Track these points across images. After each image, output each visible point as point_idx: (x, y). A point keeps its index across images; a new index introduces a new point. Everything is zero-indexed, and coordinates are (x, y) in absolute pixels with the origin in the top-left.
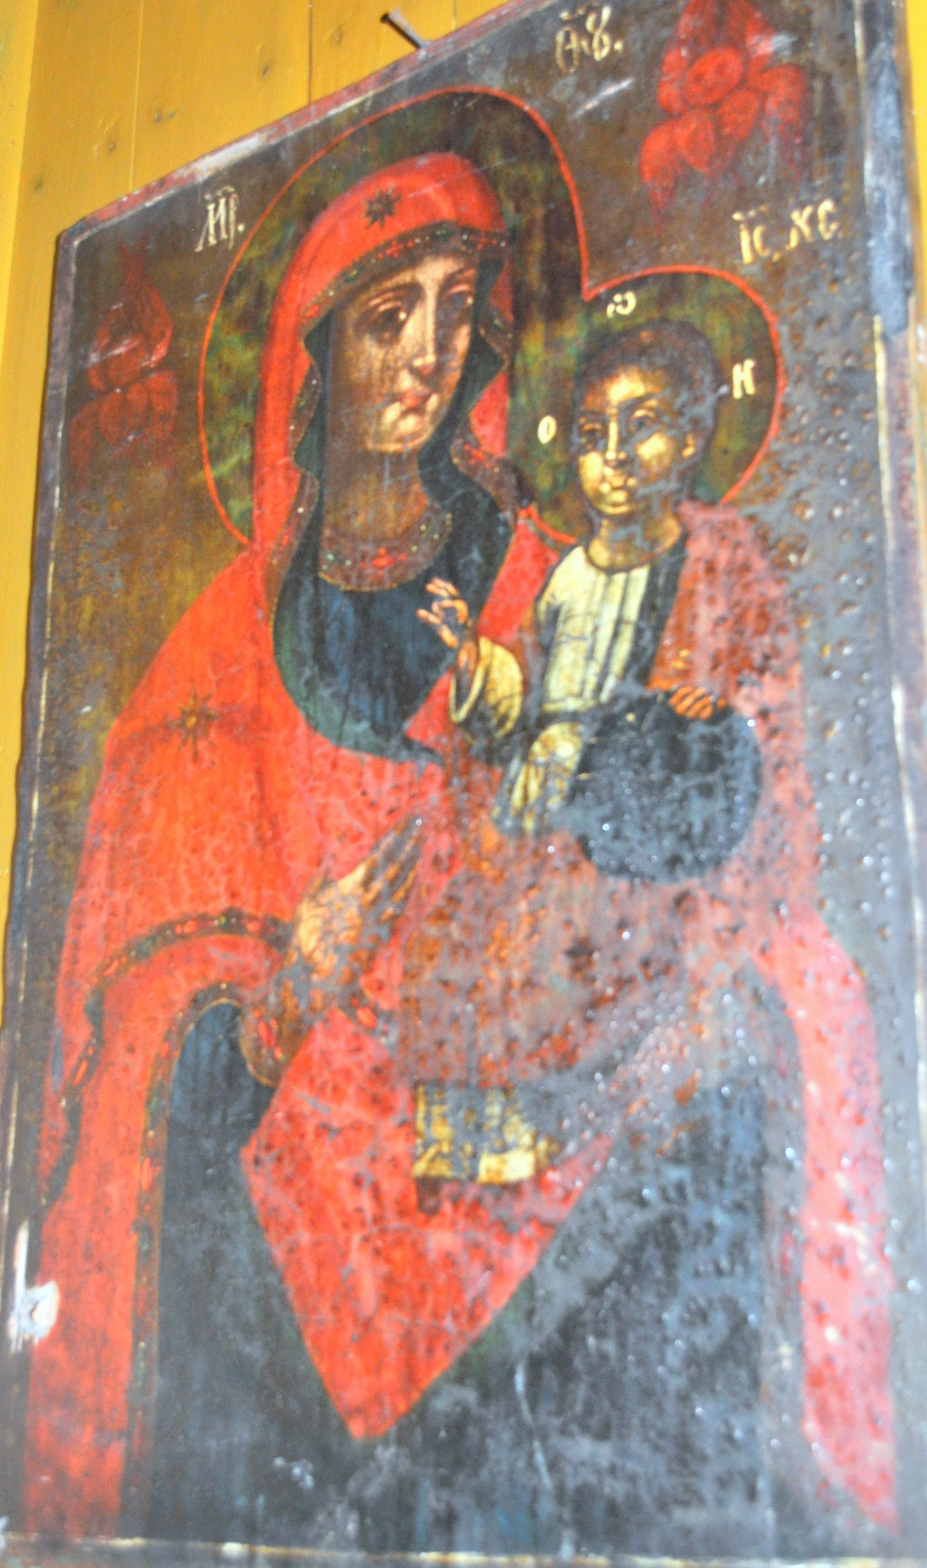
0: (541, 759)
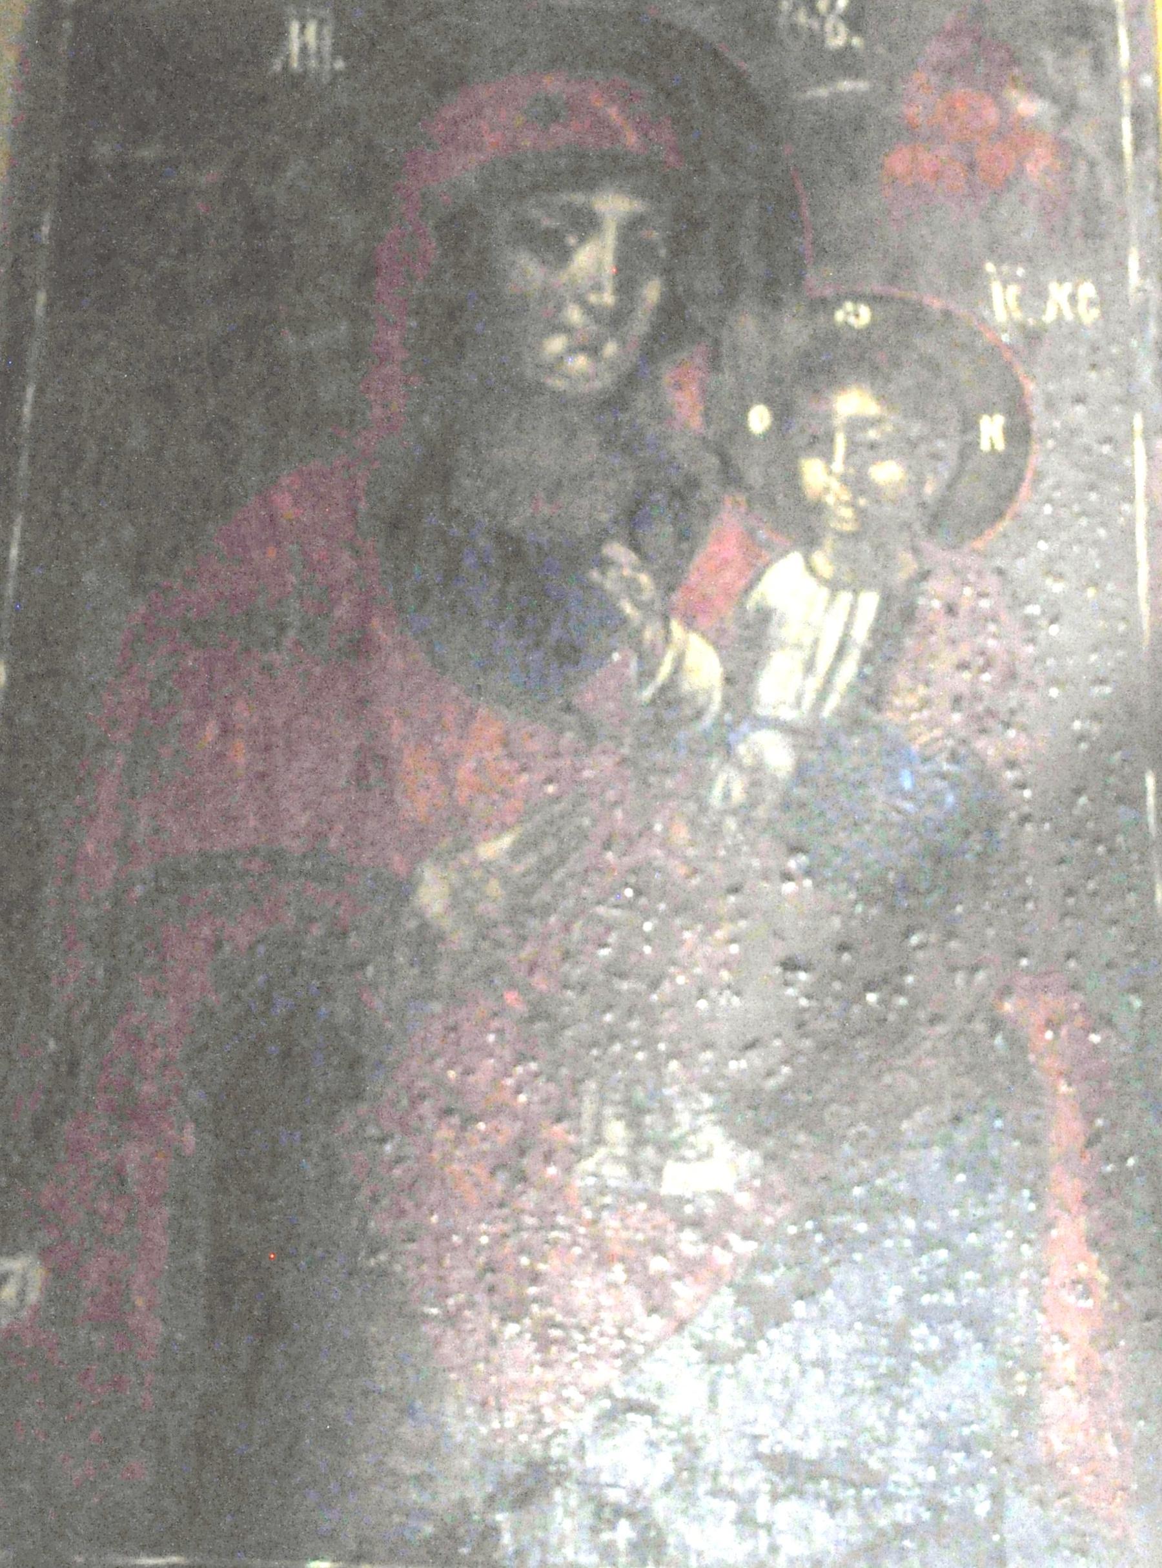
0: (748, 761)
